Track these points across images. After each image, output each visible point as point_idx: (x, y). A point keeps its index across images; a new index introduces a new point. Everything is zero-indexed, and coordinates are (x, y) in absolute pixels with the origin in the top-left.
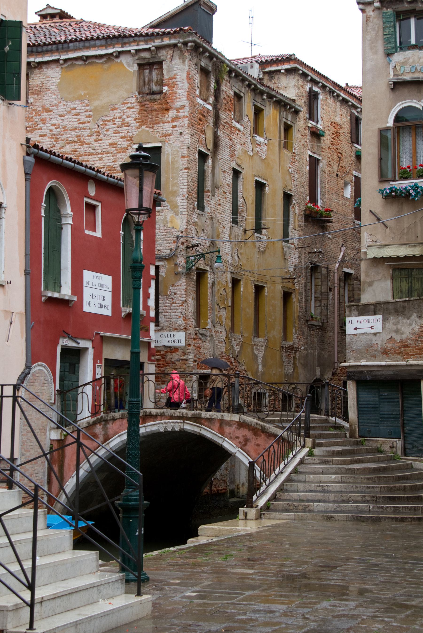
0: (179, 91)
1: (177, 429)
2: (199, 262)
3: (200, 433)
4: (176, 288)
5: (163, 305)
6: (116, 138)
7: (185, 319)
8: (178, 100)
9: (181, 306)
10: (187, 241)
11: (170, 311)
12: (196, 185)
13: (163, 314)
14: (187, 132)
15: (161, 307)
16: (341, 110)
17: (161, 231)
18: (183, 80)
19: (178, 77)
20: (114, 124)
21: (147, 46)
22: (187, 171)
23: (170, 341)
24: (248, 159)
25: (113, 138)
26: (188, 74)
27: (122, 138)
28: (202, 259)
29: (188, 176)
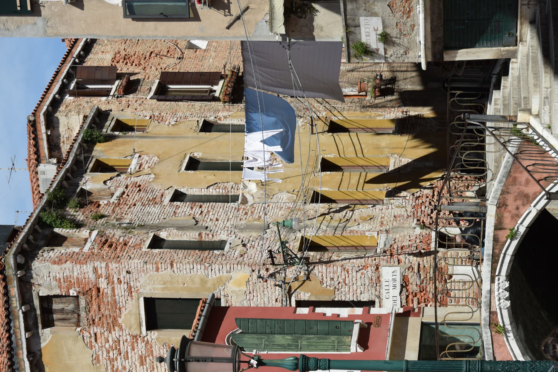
0: (76, 274)
1: (507, 284)
2: (291, 248)
3: (512, 256)
4: (325, 279)
5: (348, 296)
6: (134, 357)
7: (365, 267)
8: (87, 276)
9: (348, 272)
10: (264, 264)
11: (355, 286)
12: (192, 252)
13: (358, 295)
14: (125, 264)
15: (349, 298)
16: (97, 53)
17: (252, 298)
18: (61, 269)
19: (58, 275)
20: (117, 360)
21: (21, 316)
22: (175, 265)
23: (395, 287)
24: (158, 180)
25: (134, 360)
26: (54, 263)
27: (133, 349)
28: (287, 245)
29: (181, 262)
